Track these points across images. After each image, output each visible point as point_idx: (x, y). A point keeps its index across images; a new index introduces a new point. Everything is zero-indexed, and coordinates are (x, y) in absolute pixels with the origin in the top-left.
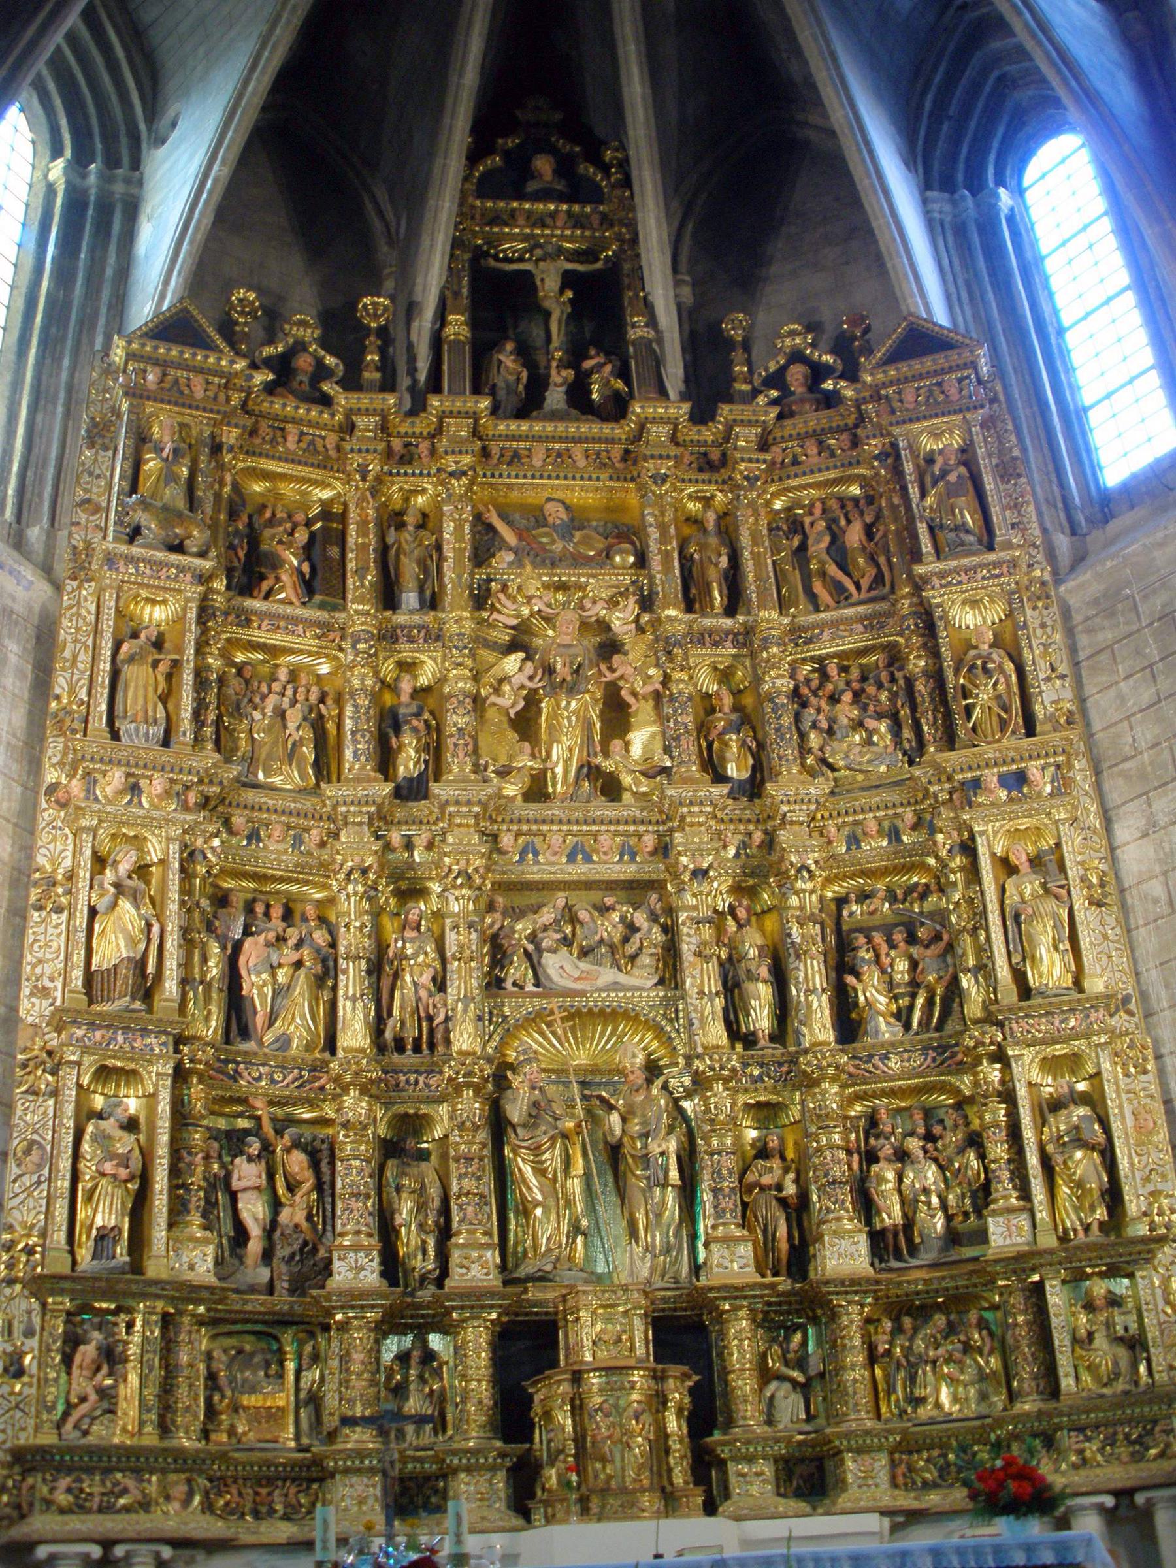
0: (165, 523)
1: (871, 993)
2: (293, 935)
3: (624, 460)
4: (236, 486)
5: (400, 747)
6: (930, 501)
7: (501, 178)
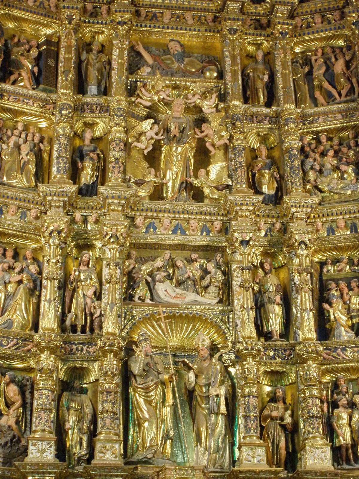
1: (338, 314)
2: (18, 266)
5: (83, 169)
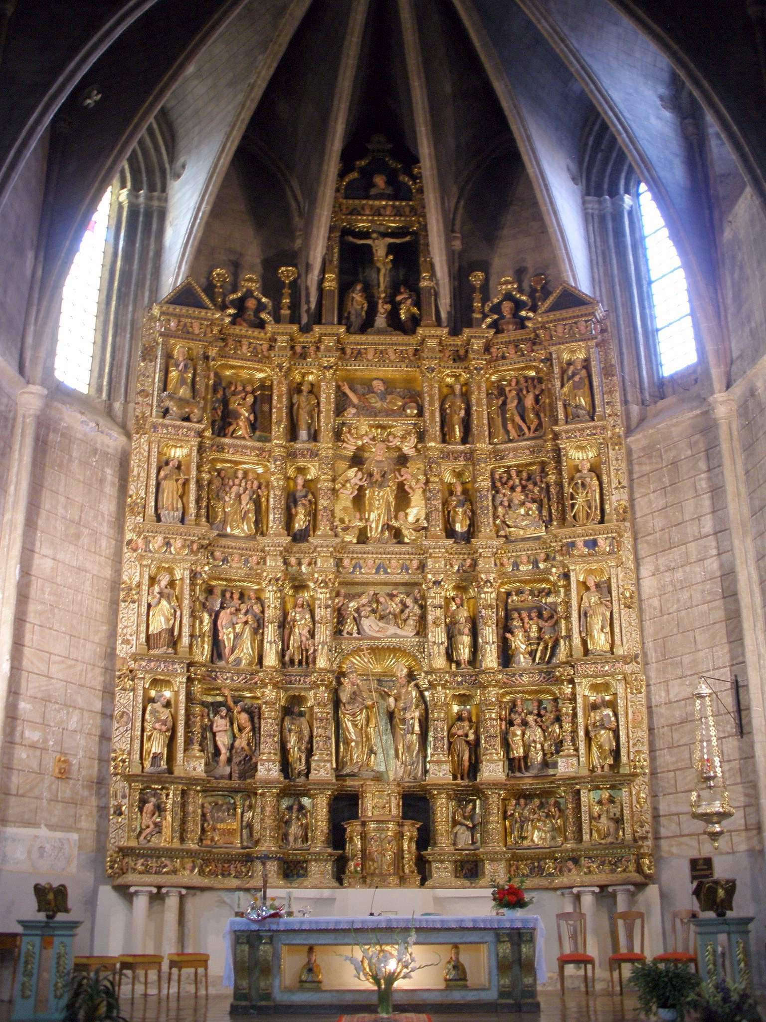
0: (180, 407)
2: (244, 608)
3: (415, 355)
4: (217, 375)
5: (297, 513)
6: (565, 389)
7: (357, 189)
